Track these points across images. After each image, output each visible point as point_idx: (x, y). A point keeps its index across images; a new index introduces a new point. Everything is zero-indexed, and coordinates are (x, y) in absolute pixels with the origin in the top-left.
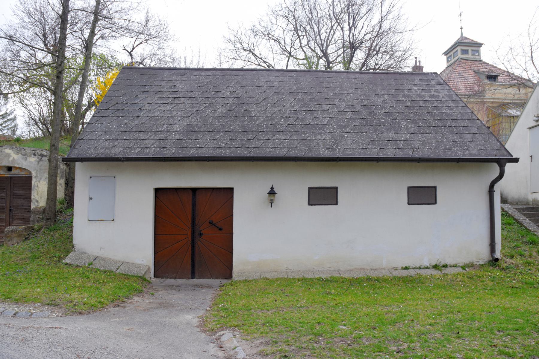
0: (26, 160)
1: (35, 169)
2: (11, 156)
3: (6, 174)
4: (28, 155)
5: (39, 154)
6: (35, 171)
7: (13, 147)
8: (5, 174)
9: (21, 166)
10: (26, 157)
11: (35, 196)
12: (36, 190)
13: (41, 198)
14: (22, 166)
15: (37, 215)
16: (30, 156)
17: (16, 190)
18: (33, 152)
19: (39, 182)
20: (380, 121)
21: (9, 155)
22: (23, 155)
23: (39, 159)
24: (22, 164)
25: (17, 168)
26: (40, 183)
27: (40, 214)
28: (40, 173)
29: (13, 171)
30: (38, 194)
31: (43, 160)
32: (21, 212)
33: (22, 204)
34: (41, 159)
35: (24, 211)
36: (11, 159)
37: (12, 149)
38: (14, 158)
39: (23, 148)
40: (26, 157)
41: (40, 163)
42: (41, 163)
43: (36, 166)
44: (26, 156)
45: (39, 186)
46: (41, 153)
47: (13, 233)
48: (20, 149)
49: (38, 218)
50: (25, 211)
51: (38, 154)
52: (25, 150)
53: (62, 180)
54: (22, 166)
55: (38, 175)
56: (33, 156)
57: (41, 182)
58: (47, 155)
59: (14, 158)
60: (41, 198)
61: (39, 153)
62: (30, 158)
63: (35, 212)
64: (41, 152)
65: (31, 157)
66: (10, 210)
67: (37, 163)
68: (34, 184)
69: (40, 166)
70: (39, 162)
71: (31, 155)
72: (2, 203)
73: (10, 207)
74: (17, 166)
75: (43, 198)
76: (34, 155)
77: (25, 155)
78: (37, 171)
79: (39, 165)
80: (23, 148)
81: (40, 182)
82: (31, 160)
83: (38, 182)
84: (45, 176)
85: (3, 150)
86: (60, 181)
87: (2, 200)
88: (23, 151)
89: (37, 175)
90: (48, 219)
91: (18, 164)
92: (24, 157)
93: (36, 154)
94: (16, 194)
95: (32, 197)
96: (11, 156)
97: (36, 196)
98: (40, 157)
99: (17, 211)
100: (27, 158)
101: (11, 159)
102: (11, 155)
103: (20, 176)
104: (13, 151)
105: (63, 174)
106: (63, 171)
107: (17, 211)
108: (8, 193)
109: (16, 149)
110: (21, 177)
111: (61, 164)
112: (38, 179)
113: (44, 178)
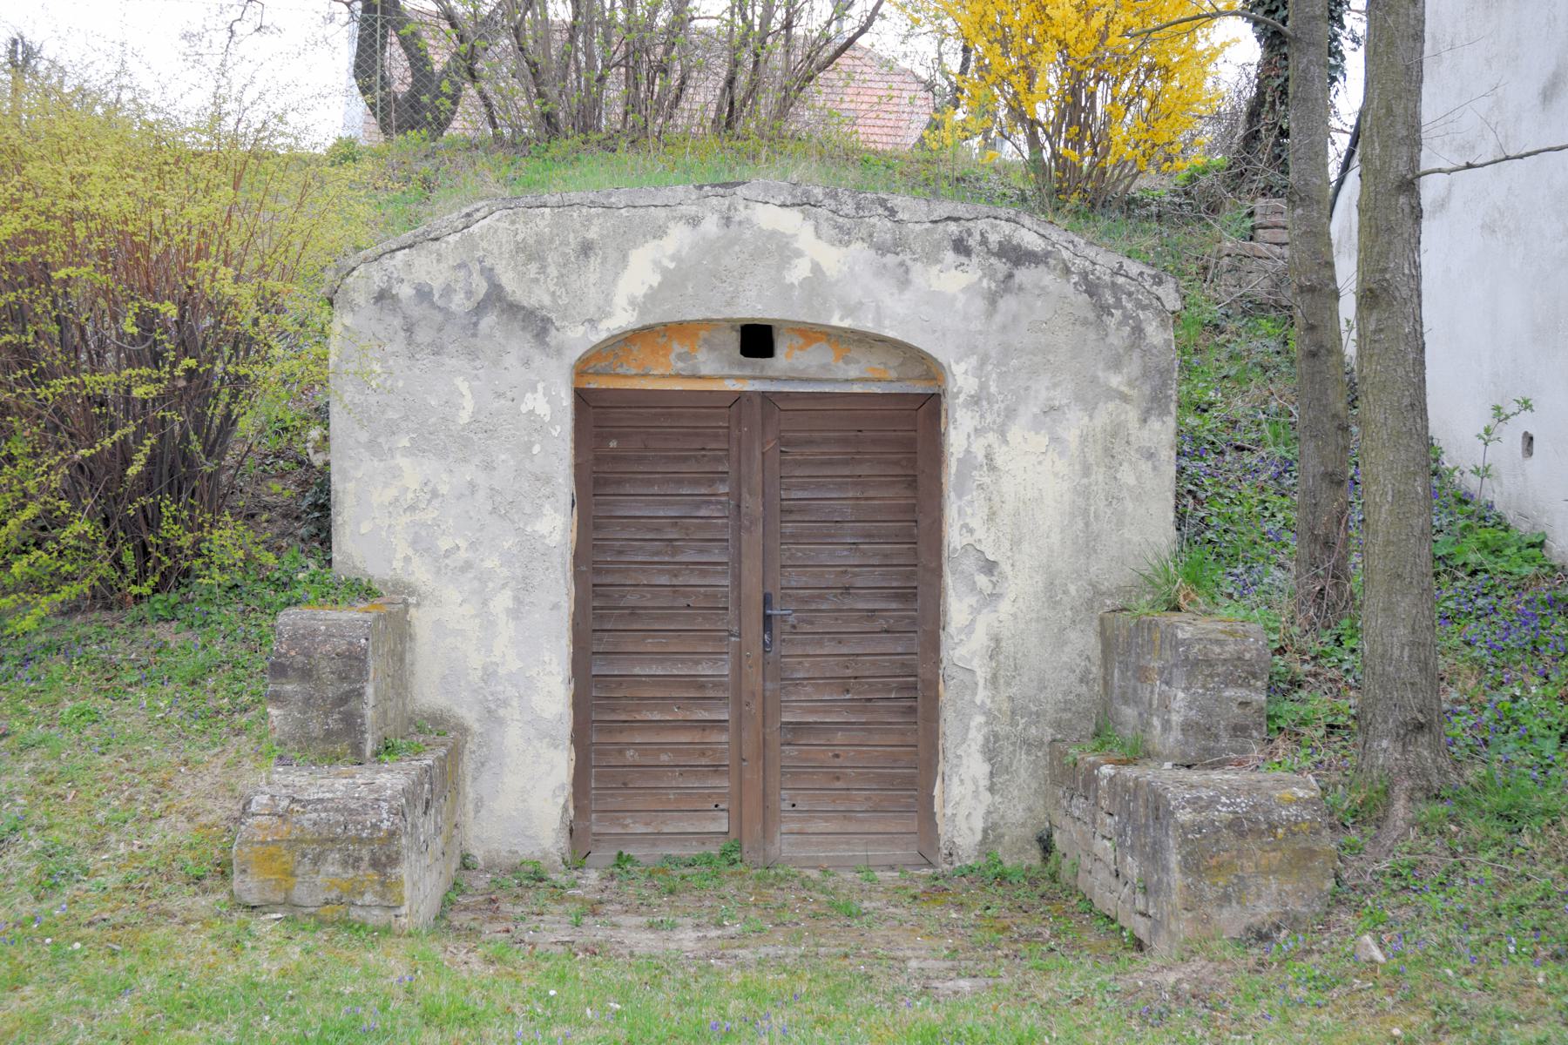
0: (904, 282)
1: (972, 350)
2: (799, 254)
3: (736, 372)
4: (917, 247)
5: (994, 247)
6: (973, 360)
7: (806, 193)
8: (726, 371)
9: (868, 324)
10: (902, 264)
11: (971, 531)
12: (980, 486)
13: (1016, 543)
14: (879, 319)
15: (1230, 680)
16: (932, 257)
17: (802, 487)
18: (953, 227)
19: (1002, 434)
20: (1083, 110)
21: (781, 250)
22: (882, 249)
23: (992, 277)
24: (878, 307)
25: (812, 334)
26: (1006, 442)
27: (1254, 676)
28: (1001, 375)
29: (787, 358)
30: (992, 516)
31: (1020, 288)
32: (838, 637)
33: (846, 581)
34: (1010, 276)
35: (855, 627)
36: (799, 272)
37: (805, 204)
38: (816, 268)
39: (883, 203)
40: (902, 264)
41: (1002, 304)
42: (1008, 304)
43: (976, 325)
44: (906, 257)
45: (999, 461)
46: (1009, 239)
47: (1250, 843)
48: (858, 207)
49: (1244, 704)
50: (867, 626)
51: (984, 241)
52: (892, 212)
53: (1155, 424)
54: (879, 319)
55: (993, 389)
56: (950, 256)
57: (1015, 433)
58: (1048, 254)
59: (816, 268)
60: (1016, 543)
61: (994, 238)
62: (935, 269)
63: (1209, 663)
64: (1007, 228)
65: (938, 261)
66: (767, 619)
67: (980, 304)
68: (968, 451)
69: (1004, 328)
70: (993, 299)
71: (938, 247)
72: (703, 574)
73: (767, 601)
74: (846, 324)
75: (1025, 546)
76: (961, 247)
77: (897, 246)
78: (983, 362)
79: (999, 319)
80: (883, 203)
81: (1009, 437)
82: (936, 285)
83: (992, 437)
84: (1043, 394)
85: (741, 213)
86: (1145, 433)
87: (701, 551)
88: (882, 226)
89: (983, 386)
90: (1420, 727)
91: (849, 311)
92: (890, 259)
93: (972, 242)
94: (801, 511)
95: (953, 537)
96: (799, 254)
97: (980, 533)
98: (1002, 267)
99: (808, 628)
100: (907, 271)
101: (799, 272)
102: (799, 244)
103: (827, 389)
104: (806, 216)
105: (1165, 384)
106: (1164, 364)
107: (808, 628)
108: (752, 504)
109: (833, 204)
110: (788, 393)
111: (1149, 314)
112: (989, 419)
113: (1036, 410)
